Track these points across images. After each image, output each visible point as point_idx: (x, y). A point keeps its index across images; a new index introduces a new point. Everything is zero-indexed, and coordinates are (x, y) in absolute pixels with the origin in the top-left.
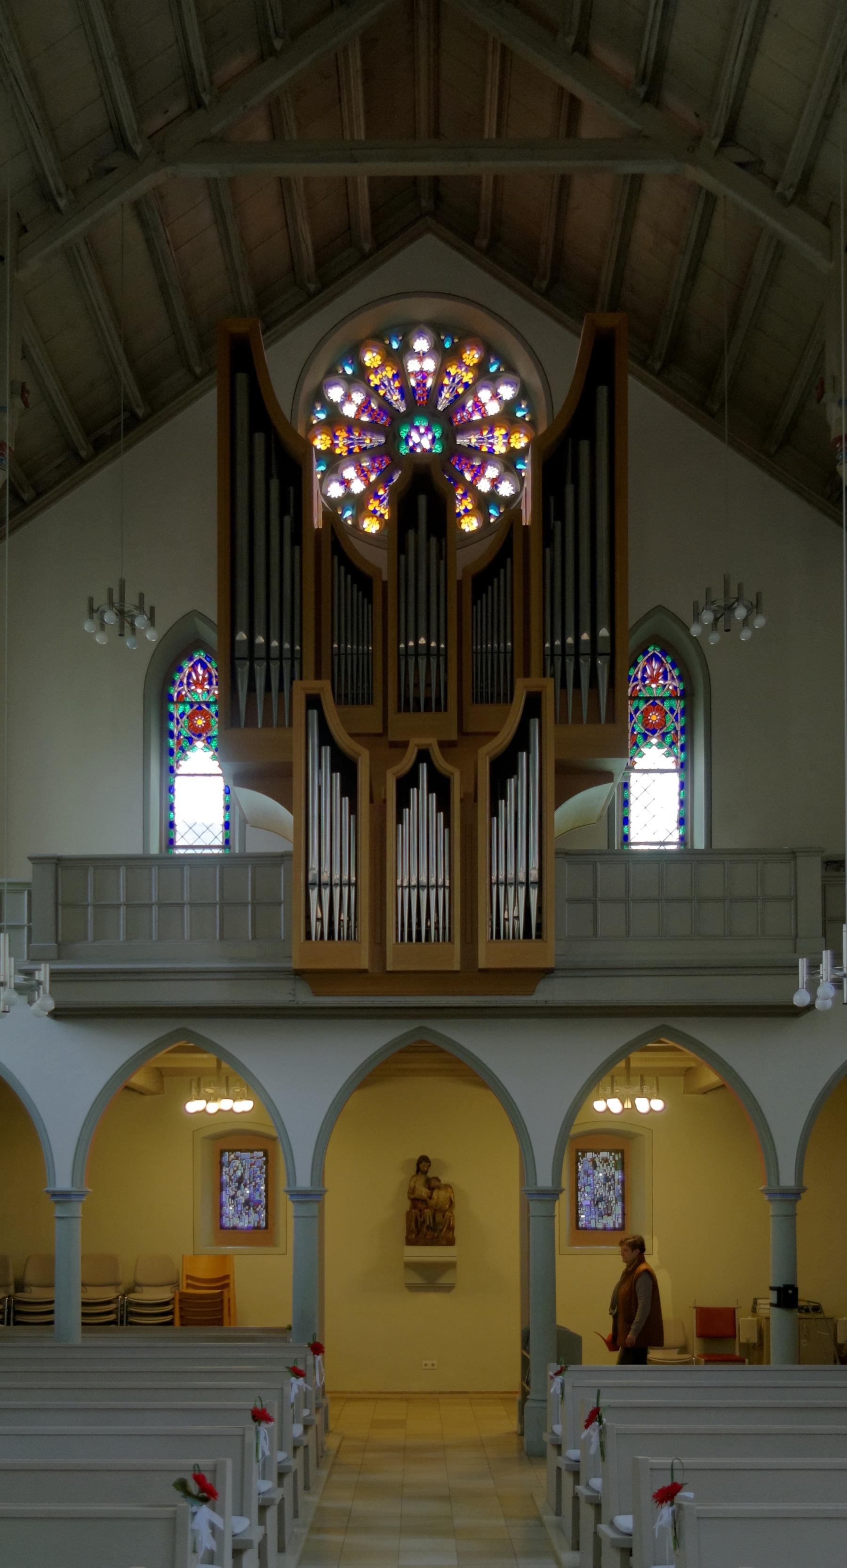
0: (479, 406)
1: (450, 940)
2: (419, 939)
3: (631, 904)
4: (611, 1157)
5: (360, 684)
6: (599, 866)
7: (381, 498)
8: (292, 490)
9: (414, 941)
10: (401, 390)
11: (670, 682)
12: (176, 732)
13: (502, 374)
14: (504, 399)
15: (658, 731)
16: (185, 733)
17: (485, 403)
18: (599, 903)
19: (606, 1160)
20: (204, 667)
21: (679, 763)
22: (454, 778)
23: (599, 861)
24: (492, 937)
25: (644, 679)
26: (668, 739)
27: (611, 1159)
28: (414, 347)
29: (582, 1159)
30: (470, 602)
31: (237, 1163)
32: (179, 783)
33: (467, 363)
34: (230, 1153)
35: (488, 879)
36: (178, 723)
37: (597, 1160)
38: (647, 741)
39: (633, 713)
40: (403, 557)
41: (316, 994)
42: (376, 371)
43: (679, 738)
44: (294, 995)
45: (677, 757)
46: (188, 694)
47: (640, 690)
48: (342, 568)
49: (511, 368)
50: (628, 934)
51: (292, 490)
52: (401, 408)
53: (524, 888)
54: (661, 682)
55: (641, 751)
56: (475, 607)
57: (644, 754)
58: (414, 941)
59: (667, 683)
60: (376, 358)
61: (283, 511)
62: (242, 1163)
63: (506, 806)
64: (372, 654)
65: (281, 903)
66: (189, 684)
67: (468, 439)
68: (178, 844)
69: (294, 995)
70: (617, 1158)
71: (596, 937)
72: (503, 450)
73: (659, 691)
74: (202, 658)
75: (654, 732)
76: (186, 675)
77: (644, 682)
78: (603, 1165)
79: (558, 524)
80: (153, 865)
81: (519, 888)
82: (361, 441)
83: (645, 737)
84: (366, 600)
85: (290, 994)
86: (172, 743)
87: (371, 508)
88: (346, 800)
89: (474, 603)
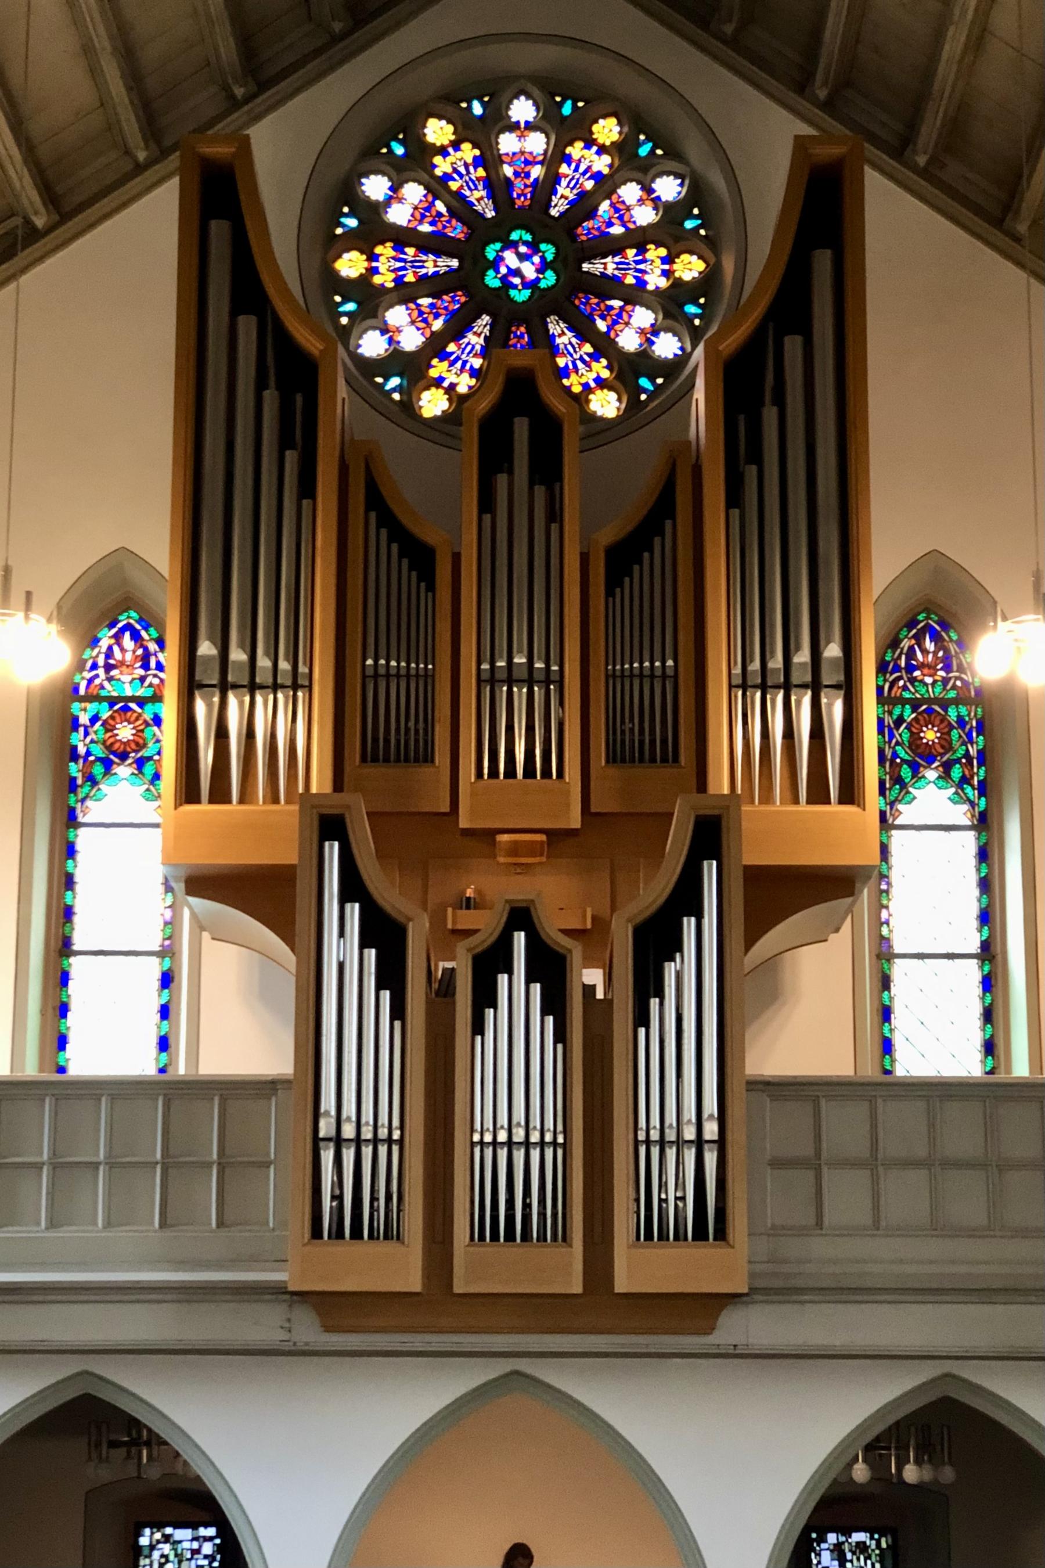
0: (621, 211)
1: (564, 1239)
2: (510, 1236)
3: (881, 1169)
4: (874, 1542)
5: (411, 724)
6: (823, 1102)
7: (452, 358)
8: (299, 399)
9: (502, 1240)
10: (488, 183)
11: (957, 674)
12: (82, 750)
13: (661, 161)
14: (663, 199)
15: (939, 758)
16: (98, 751)
17: (630, 206)
18: (825, 1170)
19: (861, 1547)
20: (136, 637)
21: (977, 814)
22: (572, 958)
23: (823, 1096)
24: (638, 1238)
25: (910, 669)
26: (956, 772)
27: (873, 1546)
28: (510, 113)
29: (819, 1545)
30: (602, 588)
31: (166, 1548)
32: (83, 839)
33: (601, 141)
34: (155, 1530)
35: (631, 1136)
36: (86, 734)
37: (846, 1547)
38: (920, 775)
39: (892, 725)
40: (487, 518)
41: (328, 1329)
42: (443, 152)
43: (975, 770)
44: (290, 1331)
45: (972, 804)
46: (106, 684)
47: (905, 688)
48: (384, 532)
49: (674, 153)
50: (876, 1224)
51: (299, 399)
52: (487, 210)
53: (693, 1150)
54: (942, 673)
55: (908, 792)
56: (611, 599)
57: (915, 798)
58: (502, 1240)
59: (951, 675)
60: (445, 131)
61: (285, 442)
62: (175, 1550)
63: (661, 1004)
64: (433, 676)
65: (271, 1163)
66: (108, 668)
67: (602, 264)
68: (75, 948)
69: (290, 1331)
70: (884, 1545)
71: (821, 1229)
72: (663, 283)
73: (938, 689)
74: (132, 621)
75: (930, 760)
76: (104, 649)
77: (911, 673)
78: (858, 1559)
79: (754, 468)
80: (47, 1095)
81: (686, 1151)
82: (420, 264)
83: (915, 768)
84: (423, 585)
85: (282, 1327)
86: (74, 769)
87: (433, 373)
88: (386, 995)
89: (610, 593)
